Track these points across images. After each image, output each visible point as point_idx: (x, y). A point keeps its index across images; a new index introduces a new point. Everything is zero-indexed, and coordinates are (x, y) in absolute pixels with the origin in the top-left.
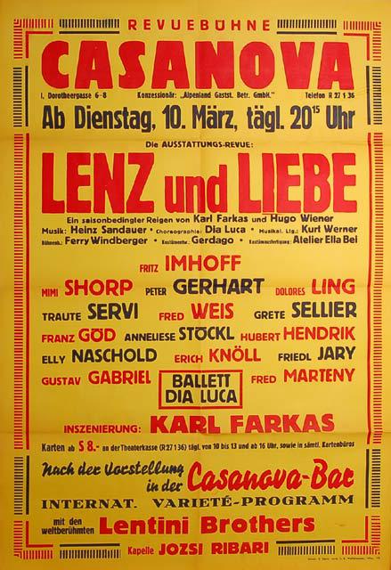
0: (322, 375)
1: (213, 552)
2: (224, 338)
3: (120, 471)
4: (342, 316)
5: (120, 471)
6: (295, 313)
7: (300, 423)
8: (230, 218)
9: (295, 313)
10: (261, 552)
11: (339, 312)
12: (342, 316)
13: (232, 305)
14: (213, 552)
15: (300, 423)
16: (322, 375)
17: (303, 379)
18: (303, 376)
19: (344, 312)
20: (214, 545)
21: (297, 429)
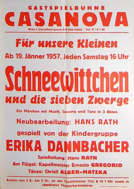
0: (110, 122)
1: (82, 159)
2: (41, 166)
3: (88, 57)
4: (11, 150)
5: (88, 57)
6: (84, 58)
7: (103, 172)
8: (43, 121)
9: (84, 58)
10: (115, 167)
11: (117, 149)
12: (11, 150)
13: (38, 158)
14: (82, 159)
15: (103, 172)
16: (110, 122)
17: (83, 123)
18: (83, 122)
19: (13, 147)
20: (82, 157)
21: (102, 173)
